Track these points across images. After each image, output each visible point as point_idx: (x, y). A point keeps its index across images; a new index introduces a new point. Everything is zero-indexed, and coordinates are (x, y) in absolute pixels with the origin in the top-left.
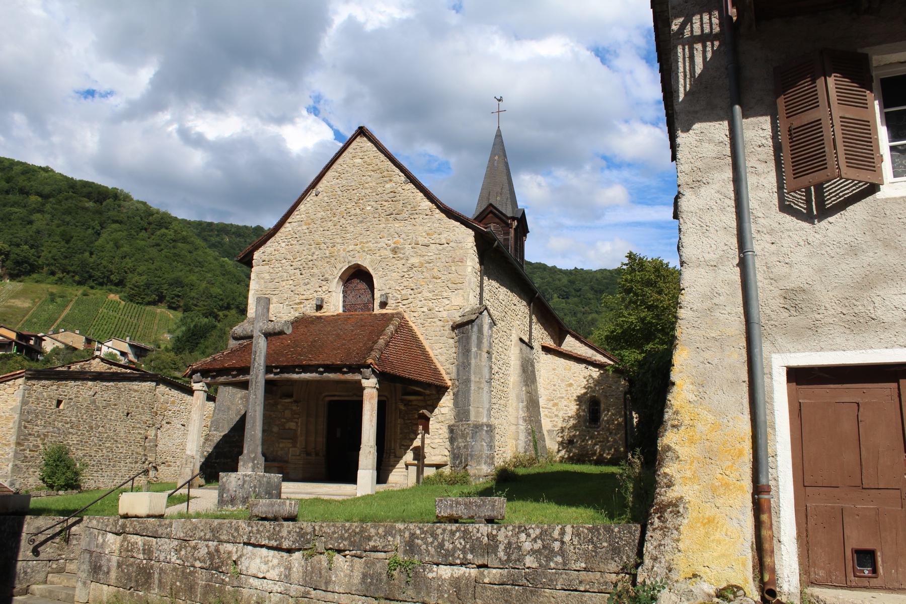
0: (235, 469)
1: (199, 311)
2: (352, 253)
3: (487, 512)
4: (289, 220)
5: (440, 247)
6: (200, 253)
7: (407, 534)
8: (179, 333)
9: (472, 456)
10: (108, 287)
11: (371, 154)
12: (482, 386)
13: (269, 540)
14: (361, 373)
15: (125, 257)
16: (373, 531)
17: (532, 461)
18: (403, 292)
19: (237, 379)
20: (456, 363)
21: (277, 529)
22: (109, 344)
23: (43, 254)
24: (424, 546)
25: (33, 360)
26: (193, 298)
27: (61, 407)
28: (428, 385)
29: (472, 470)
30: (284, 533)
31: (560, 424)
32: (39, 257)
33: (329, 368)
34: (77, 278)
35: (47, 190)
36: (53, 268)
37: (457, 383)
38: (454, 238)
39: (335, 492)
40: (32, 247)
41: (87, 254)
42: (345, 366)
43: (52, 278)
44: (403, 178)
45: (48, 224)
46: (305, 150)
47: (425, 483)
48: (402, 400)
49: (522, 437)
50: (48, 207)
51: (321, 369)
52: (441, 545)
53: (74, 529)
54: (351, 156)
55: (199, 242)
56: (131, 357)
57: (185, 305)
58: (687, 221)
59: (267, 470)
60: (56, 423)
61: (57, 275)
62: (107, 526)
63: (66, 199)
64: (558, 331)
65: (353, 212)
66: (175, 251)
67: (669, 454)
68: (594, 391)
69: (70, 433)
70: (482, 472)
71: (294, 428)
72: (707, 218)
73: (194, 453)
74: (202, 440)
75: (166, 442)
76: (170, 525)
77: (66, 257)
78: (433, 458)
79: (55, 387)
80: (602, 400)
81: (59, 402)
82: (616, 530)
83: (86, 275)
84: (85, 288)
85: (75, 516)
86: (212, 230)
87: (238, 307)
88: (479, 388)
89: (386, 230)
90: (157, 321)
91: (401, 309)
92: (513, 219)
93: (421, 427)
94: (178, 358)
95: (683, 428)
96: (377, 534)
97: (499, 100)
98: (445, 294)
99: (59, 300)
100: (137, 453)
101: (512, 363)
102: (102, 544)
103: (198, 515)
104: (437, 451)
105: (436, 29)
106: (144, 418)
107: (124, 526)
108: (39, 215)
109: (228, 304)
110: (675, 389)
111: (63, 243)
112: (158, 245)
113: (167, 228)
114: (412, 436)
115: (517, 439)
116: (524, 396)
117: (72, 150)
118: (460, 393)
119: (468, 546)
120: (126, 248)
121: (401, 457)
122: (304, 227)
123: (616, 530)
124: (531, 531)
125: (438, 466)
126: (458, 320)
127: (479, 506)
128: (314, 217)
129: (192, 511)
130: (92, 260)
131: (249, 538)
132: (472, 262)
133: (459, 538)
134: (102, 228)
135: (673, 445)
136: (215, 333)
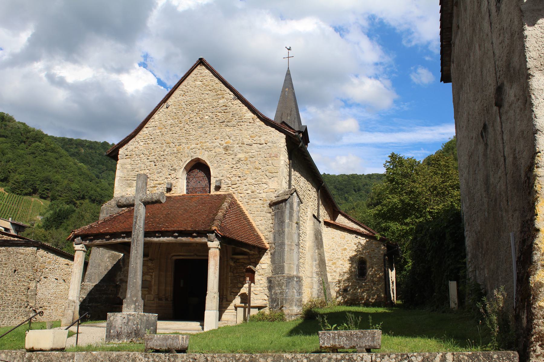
0: (120, 310)
1: (62, 200)
2: (194, 150)
4: (146, 126)
6: (64, 159)
8: (48, 215)
9: (286, 300)
11: (208, 79)
12: (293, 248)
14: (207, 237)
15: (9, 161)
17: (323, 304)
18: (233, 179)
19: (110, 241)
20: (273, 231)
21: (172, 359)
28: (253, 247)
29: (286, 311)
31: (338, 278)
33: (182, 233)
37: (273, 246)
38: (271, 140)
39: (182, 328)
42: (195, 231)
44: (232, 96)
46: (137, 91)
48: (232, 259)
49: (316, 287)
51: (176, 234)
54: (193, 79)
55: (63, 151)
56: (12, 232)
57: (52, 196)
58: (538, 97)
64: (334, 212)
65: (195, 120)
68: (362, 254)
70: (293, 312)
71: (149, 279)
75: (46, 290)
78: (256, 302)
80: (368, 260)
82: (495, 356)
86: (72, 144)
87: (90, 198)
88: (291, 250)
90: (31, 207)
91: (231, 191)
92: (299, 132)
93: (248, 278)
94: (47, 233)
97: (289, 49)
98: (264, 181)
100: (21, 300)
101: (308, 232)
103: (89, 349)
105: (229, 12)
106: (27, 274)
109: (83, 195)
112: (33, 153)
113: (40, 142)
114: (240, 285)
116: (317, 257)
118: (276, 253)
120: (10, 155)
121: (231, 301)
122: (158, 131)
123: (495, 356)
125: (260, 308)
126: (274, 199)
127: (360, 338)
128: (166, 123)
132: (284, 158)
136: (74, 215)
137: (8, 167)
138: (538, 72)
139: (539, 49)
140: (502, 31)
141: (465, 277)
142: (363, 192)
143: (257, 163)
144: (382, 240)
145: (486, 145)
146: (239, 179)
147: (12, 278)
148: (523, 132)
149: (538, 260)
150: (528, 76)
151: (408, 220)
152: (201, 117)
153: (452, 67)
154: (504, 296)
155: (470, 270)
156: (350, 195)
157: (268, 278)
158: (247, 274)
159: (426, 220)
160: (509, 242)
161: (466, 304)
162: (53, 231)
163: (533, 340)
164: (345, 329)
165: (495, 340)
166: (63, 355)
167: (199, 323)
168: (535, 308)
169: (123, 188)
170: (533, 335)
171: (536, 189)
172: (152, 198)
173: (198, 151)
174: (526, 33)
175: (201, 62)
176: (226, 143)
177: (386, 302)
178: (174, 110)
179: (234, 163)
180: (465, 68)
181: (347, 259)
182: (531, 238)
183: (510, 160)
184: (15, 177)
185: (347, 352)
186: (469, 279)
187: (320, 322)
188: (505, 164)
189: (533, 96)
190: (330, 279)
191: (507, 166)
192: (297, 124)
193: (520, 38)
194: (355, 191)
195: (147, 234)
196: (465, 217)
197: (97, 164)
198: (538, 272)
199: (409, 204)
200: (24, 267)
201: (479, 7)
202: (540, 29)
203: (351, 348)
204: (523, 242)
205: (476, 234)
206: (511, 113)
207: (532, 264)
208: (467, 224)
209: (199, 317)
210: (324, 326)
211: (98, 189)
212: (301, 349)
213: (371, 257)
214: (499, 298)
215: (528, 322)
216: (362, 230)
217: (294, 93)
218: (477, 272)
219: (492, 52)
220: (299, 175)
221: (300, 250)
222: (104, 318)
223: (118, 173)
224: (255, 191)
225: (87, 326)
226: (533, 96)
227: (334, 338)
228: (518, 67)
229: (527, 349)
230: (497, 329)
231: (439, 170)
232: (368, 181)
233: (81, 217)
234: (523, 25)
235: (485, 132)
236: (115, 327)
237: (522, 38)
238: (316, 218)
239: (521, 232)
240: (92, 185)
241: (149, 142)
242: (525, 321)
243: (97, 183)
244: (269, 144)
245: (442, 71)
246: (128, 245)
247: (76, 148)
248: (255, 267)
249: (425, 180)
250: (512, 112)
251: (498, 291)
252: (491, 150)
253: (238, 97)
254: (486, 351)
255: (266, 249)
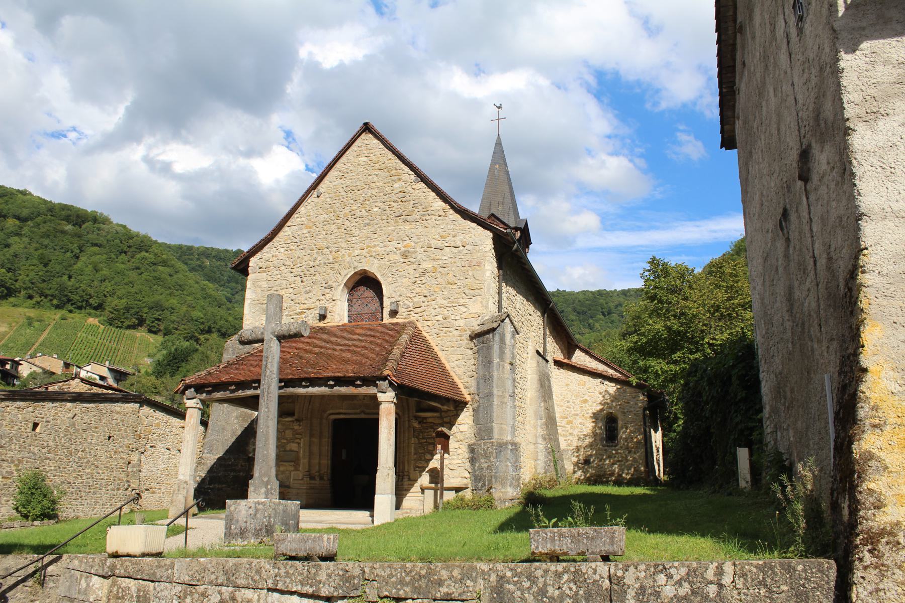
0: (244, 495)
1: (180, 334)
2: (358, 258)
3: (604, 546)
4: (288, 224)
5: (456, 250)
6: (180, 275)
7: (493, 578)
8: (159, 357)
9: (496, 477)
10: (87, 311)
12: (505, 400)
13: (302, 585)
14: (376, 386)
15: (105, 280)
16: (444, 574)
17: (553, 483)
18: (415, 300)
20: (476, 375)
21: (313, 571)
22: (88, 368)
23: (21, 277)
24: (519, 593)
25: (9, 385)
26: (173, 322)
27: (38, 430)
29: (496, 494)
30: (323, 576)
31: (575, 444)
32: (16, 281)
33: (341, 381)
34: (55, 302)
35: (25, 213)
36: (30, 291)
37: (477, 397)
38: (471, 240)
39: (343, 520)
40: (9, 270)
41: (65, 278)
42: (359, 378)
43: (30, 301)
44: (413, 176)
45: (26, 248)
46: (277, 181)
47: (445, 508)
48: (416, 418)
49: (542, 457)
50: (25, 230)
51: (331, 383)
52: (543, 592)
53: (50, 569)
54: (355, 154)
55: (180, 265)
56: (111, 382)
58: (863, 162)
59: (283, 496)
60: (32, 448)
61: (35, 299)
62: (92, 567)
63: (45, 222)
64: (569, 345)
65: (358, 214)
66: (156, 274)
67: (873, 463)
69: (47, 458)
70: (508, 496)
71: (296, 449)
72: (890, 158)
73: (187, 478)
74: (195, 464)
75: (153, 465)
76: (172, 566)
77: (44, 281)
78: (452, 481)
79: (31, 409)
80: (620, 417)
81: (35, 425)
82: (800, 567)
83: (64, 299)
84: (63, 312)
85: (51, 554)
86: (192, 254)
87: (219, 331)
88: (502, 403)
89: (395, 233)
90: (137, 345)
92: (516, 229)
93: (439, 447)
95: (888, 428)
96: (451, 577)
97: (499, 108)
98: (462, 301)
99: (36, 324)
100: (119, 479)
101: (529, 377)
102: (86, 590)
103: (202, 552)
104: (455, 473)
106: (127, 442)
107: (113, 567)
108: (16, 239)
109: (209, 327)
110: (869, 377)
111: (41, 266)
112: (138, 268)
113: (147, 252)
114: (428, 456)
115: (536, 459)
116: (542, 413)
117: (48, 178)
118: (481, 408)
119: (581, 592)
120: (105, 272)
122: (305, 231)
123: (800, 567)
124: (673, 571)
125: (458, 490)
126: (478, 329)
128: (316, 219)
129: (193, 545)
130: (70, 284)
131: (276, 583)
132: (490, 266)
133: (569, 581)
134: (81, 251)
135: (875, 451)
136: (196, 357)
137: (103, 288)
138: (861, 124)
139: (863, 88)
140: (806, 65)
141: (761, 441)
142: (615, 317)
143: (451, 275)
144: (639, 387)
145: (788, 240)
146: (425, 299)
147: (105, 448)
148: (840, 218)
149: (866, 417)
150: (847, 131)
151: (678, 355)
152: (368, 208)
153: (737, 126)
154: (813, 473)
155: (769, 430)
156: (597, 321)
157: (469, 445)
158: (437, 439)
159: (704, 355)
160: (823, 389)
161: (763, 482)
162: (167, 379)
163: (858, 542)
164: (570, 525)
165: (800, 541)
166: (159, 562)
167: (368, 513)
168: (861, 492)
169: (253, 318)
170: (858, 535)
171: (862, 306)
172: (289, 330)
173: (364, 260)
174: (842, 64)
175: (367, 128)
176: (405, 247)
177: (648, 478)
178: (328, 200)
179: (417, 275)
180: (755, 125)
181: (588, 416)
182: (854, 383)
183: (822, 262)
184: (113, 302)
185: (574, 561)
186: (767, 445)
187: (531, 515)
188: (815, 269)
189: (854, 162)
190: (563, 445)
191: (818, 271)
192: (512, 217)
193: (833, 73)
194: (604, 314)
195: (286, 382)
196: (760, 351)
197: (229, 282)
198: (865, 436)
199: (678, 333)
200: (123, 432)
201: (773, 31)
202: (864, 58)
203: (579, 554)
204: (843, 388)
205: (776, 376)
206: (823, 190)
207: (856, 424)
208: (763, 362)
209: (367, 504)
210: (538, 521)
211: (230, 319)
212: (505, 556)
213: (624, 413)
214: (805, 476)
215: (850, 513)
216: (611, 372)
217: (507, 172)
218: (779, 433)
219: (793, 97)
220: (514, 293)
221: (517, 403)
222: (223, 507)
223: (249, 294)
224: (449, 317)
225: (205, 518)
226: (854, 162)
227: (553, 540)
228: (831, 118)
229: (848, 557)
230: (803, 525)
231: (723, 281)
232: (622, 300)
233: (205, 359)
234: (837, 52)
235: (785, 221)
236: (237, 521)
237: (837, 72)
238: (541, 355)
239: (840, 374)
240: (222, 312)
241: (292, 247)
242: (846, 512)
243: (229, 309)
244: (467, 247)
245: (722, 132)
246: (257, 397)
247: (198, 259)
248: (450, 429)
249: (702, 296)
250: (825, 188)
251: (804, 466)
252: (795, 248)
253: (422, 178)
254: (786, 558)
255: (466, 403)
